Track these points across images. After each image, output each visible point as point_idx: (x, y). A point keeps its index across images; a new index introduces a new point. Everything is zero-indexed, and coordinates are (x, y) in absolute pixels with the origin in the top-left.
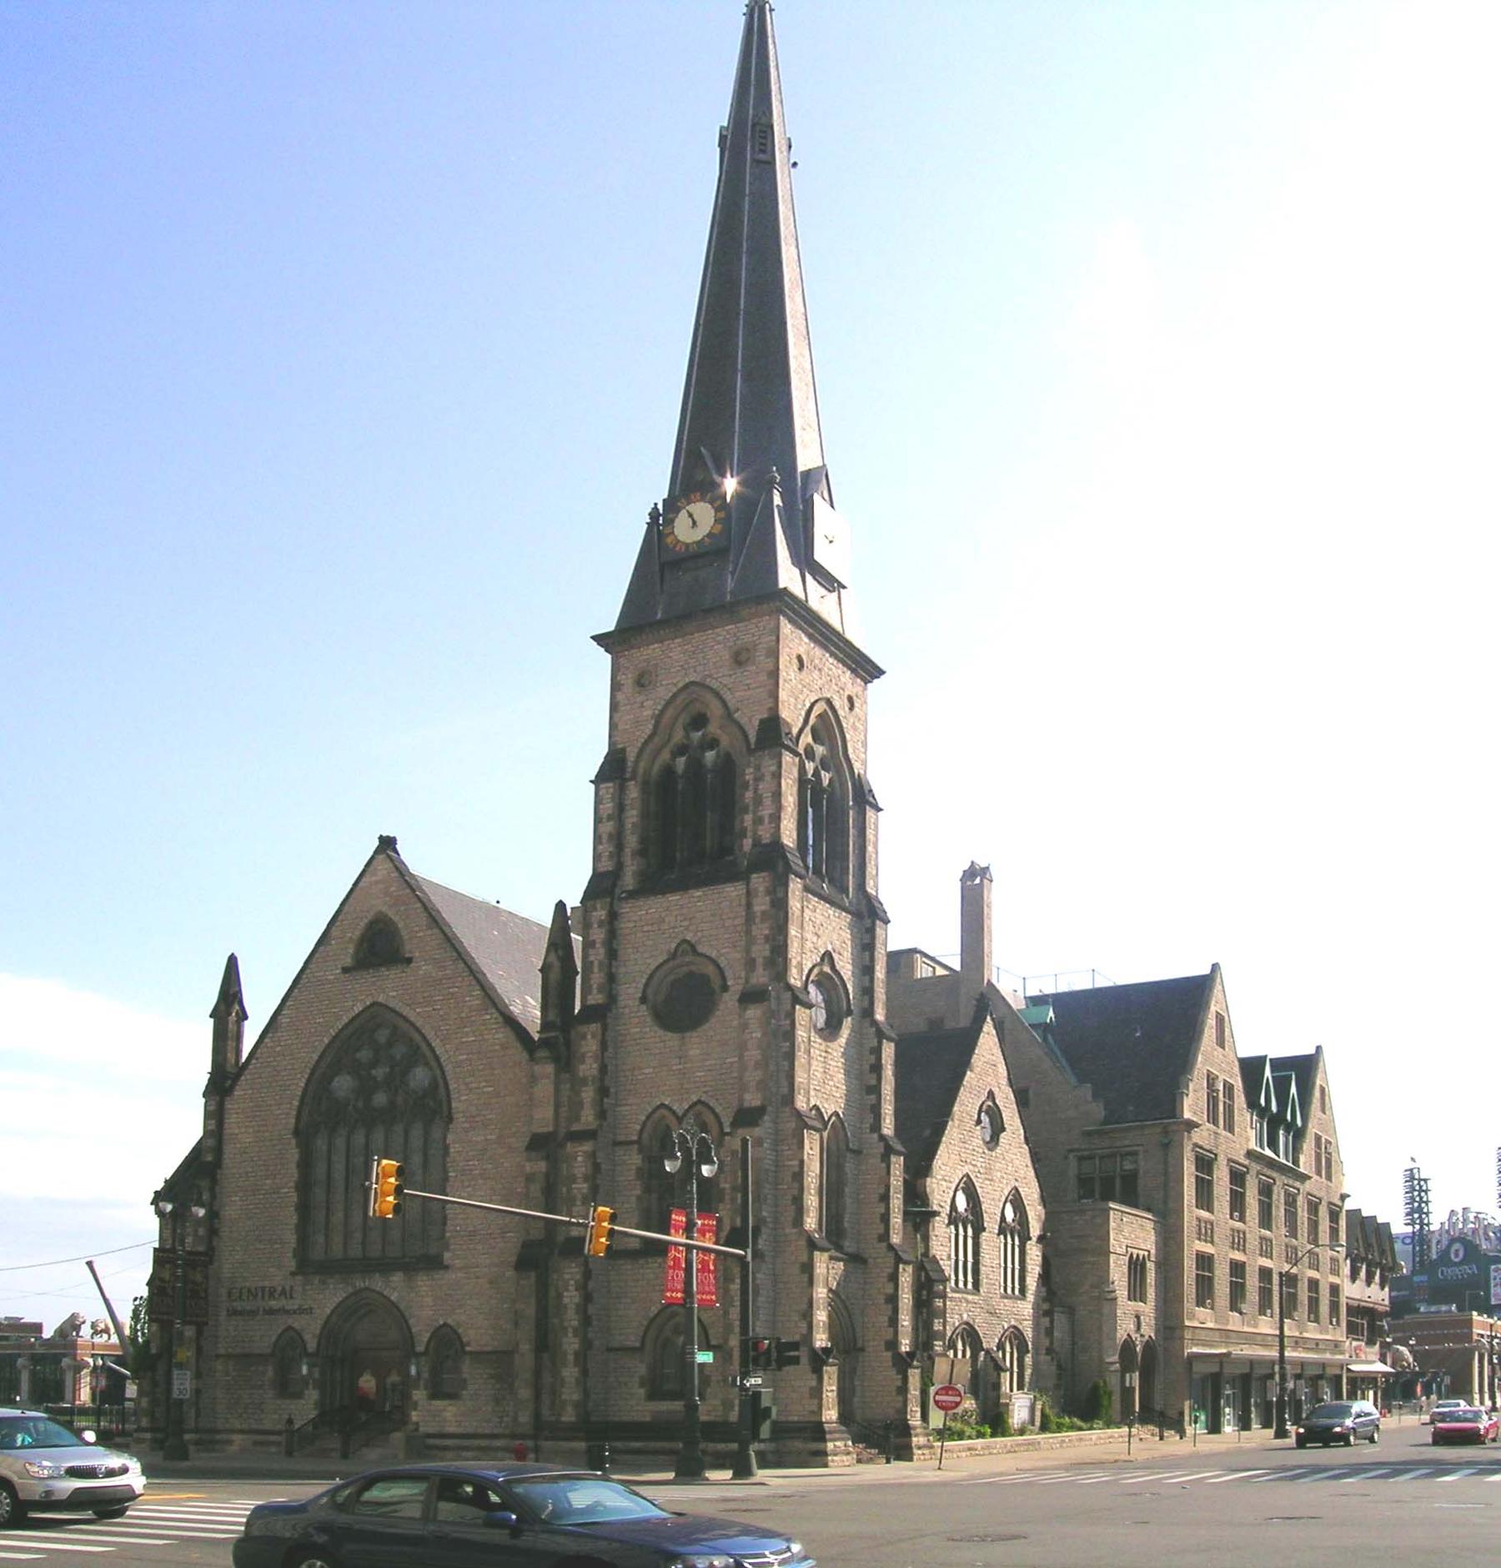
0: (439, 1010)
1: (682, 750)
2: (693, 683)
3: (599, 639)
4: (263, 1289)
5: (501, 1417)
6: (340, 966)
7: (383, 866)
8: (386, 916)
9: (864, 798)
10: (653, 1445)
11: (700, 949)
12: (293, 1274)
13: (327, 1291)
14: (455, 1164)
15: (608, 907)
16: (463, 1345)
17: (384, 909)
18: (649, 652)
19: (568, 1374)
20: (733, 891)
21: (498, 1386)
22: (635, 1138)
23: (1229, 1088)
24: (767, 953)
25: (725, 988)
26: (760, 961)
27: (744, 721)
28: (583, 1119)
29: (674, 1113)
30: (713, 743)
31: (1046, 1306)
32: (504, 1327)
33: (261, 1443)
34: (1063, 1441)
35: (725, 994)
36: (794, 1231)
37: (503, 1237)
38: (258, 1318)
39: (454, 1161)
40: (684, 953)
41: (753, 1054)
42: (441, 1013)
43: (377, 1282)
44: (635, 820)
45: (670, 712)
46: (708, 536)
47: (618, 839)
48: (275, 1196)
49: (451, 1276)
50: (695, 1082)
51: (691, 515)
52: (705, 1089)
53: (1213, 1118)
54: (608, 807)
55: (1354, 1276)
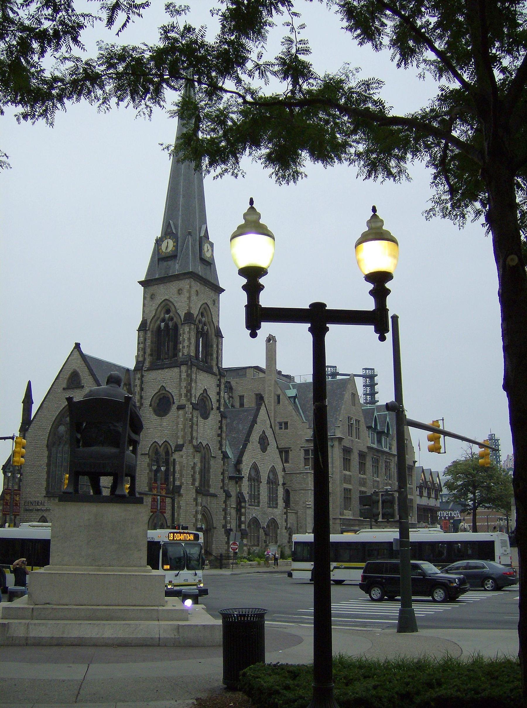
1: (163, 320)
2: (166, 300)
3: (141, 283)
4: (35, 501)
7: (76, 353)
9: (219, 335)
12: (45, 497)
15: (141, 373)
17: (76, 368)
18: (153, 289)
20: (176, 370)
22: (147, 452)
23: (358, 421)
24: (185, 392)
25: (174, 403)
26: (183, 394)
27: (180, 313)
29: (159, 445)
31: (285, 510)
34: (287, 563)
36: (192, 487)
40: (163, 390)
41: (181, 426)
44: (149, 343)
45: (159, 309)
47: (144, 350)
53: (350, 434)
54: (142, 339)
55: (421, 495)
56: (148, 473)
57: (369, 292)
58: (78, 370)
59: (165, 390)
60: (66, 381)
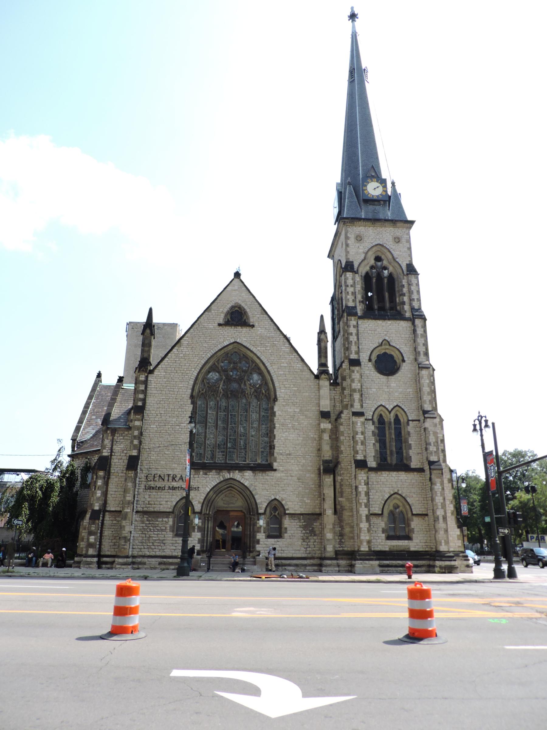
0: (269, 350)
4: (169, 475)
5: (306, 548)
6: (216, 323)
8: (240, 305)
10: (394, 562)
11: (391, 344)
13: (208, 479)
14: (278, 421)
16: (285, 510)
19: (363, 526)
21: (304, 532)
22: (371, 418)
28: (355, 407)
29: (387, 409)
30: (385, 268)
32: (306, 501)
33: (165, 564)
35: (404, 363)
37: (304, 458)
38: (166, 490)
39: (278, 420)
40: (385, 345)
42: (270, 351)
43: (236, 475)
44: (359, 289)
46: (377, 196)
48: (178, 427)
49: (277, 474)
50: (394, 397)
51: (378, 187)
52: (399, 401)
56: (374, 444)
57: (240, 307)
58: (243, 305)
59: (390, 345)
60: (223, 316)
